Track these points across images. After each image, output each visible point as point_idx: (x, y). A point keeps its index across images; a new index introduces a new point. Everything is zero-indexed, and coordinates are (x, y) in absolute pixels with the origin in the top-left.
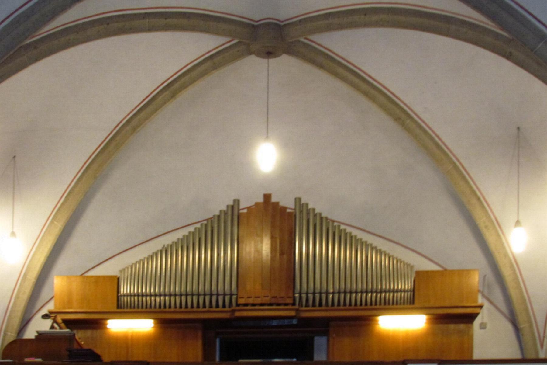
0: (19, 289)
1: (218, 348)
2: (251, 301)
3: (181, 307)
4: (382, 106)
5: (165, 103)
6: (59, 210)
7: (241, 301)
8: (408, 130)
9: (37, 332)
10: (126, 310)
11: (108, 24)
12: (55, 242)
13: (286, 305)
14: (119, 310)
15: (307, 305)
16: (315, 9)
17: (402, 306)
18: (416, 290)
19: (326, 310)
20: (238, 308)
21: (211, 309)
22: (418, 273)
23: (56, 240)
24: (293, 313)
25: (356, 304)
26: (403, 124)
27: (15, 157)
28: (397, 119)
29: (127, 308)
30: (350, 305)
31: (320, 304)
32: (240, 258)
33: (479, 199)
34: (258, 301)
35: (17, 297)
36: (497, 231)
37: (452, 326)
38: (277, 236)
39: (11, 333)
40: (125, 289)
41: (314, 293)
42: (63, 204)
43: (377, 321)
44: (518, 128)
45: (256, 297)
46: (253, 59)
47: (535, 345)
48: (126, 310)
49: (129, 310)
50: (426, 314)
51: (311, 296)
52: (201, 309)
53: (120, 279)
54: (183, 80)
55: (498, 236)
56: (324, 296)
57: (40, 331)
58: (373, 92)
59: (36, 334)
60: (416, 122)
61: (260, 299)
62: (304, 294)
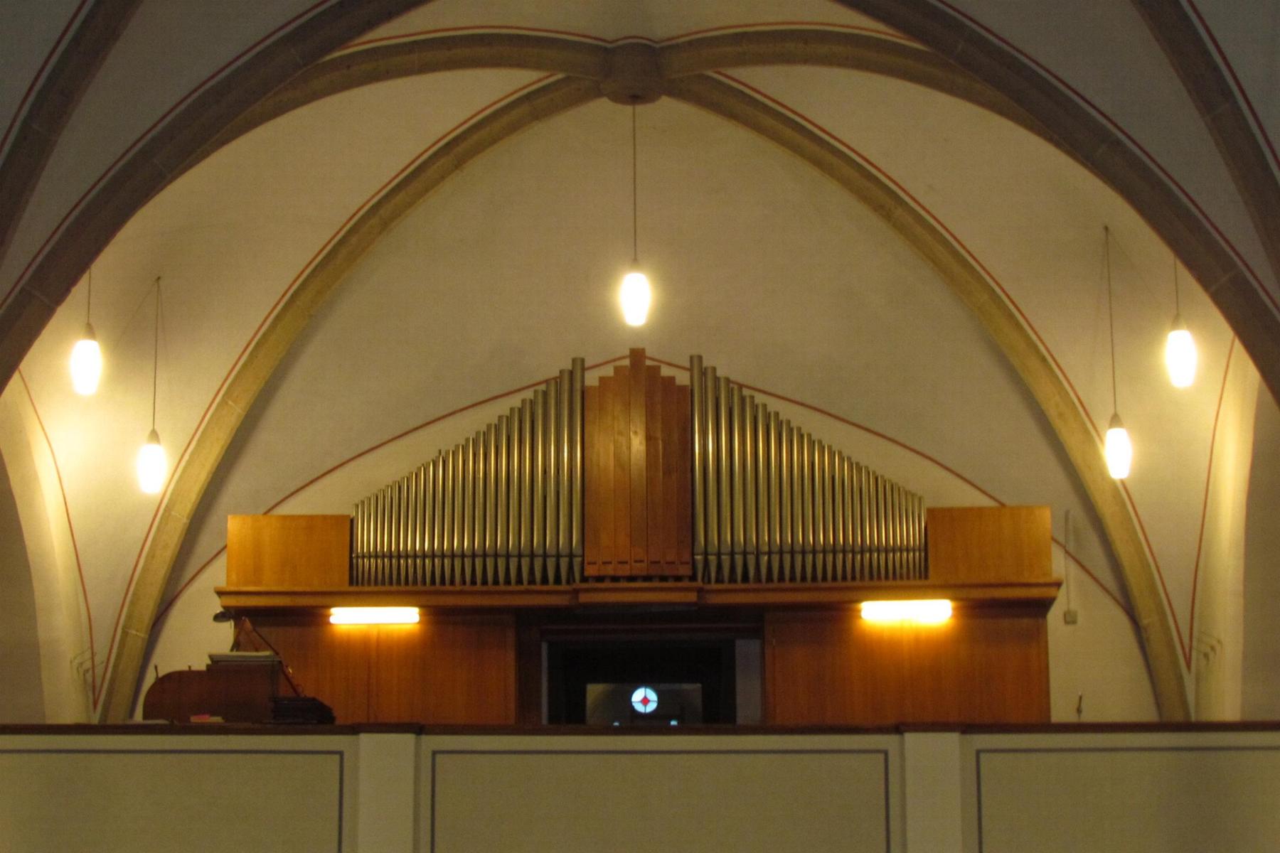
0: (154, 540)
1: (545, 664)
2: (609, 571)
3: (473, 582)
4: (845, 183)
5: (443, 178)
6: (237, 377)
7: (591, 571)
8: (900, 228)
9: (211, 657)
10: (366, 589)
11: (349, 67)
12: (229, 442)
13: (678, 578)
14: (353, 589)
17: (905, 582)
18: (930, 545)
19: (755, 591)
21: (533, 587)
22: (932, 513)
24: (692, 597)
26: (888, 216)
27: (159, 278)
28: (878, 208)
29: (369, 584)
30: (804, 578)
32: (586, 480)
33: (1044, 360)
34: (625, 571)
35: (152, 555)
36: (1083, 424)
37: (1006, 623)
38: (659, 435)
39: (137, 631)
41: (732, 554)
42: (245, 365)
43: (859, 611)
44: (1106, 229)
45: (620, 563)
48: (366, 589)
49: (372, 588)
50: (953, 599)
51: (726, 559)
52: (513, 587)
53: (355, 522)
55: (1087, 432)
57: (217, 656)
58: (830, 158)
61: (627, 567)
62: (712, 554)
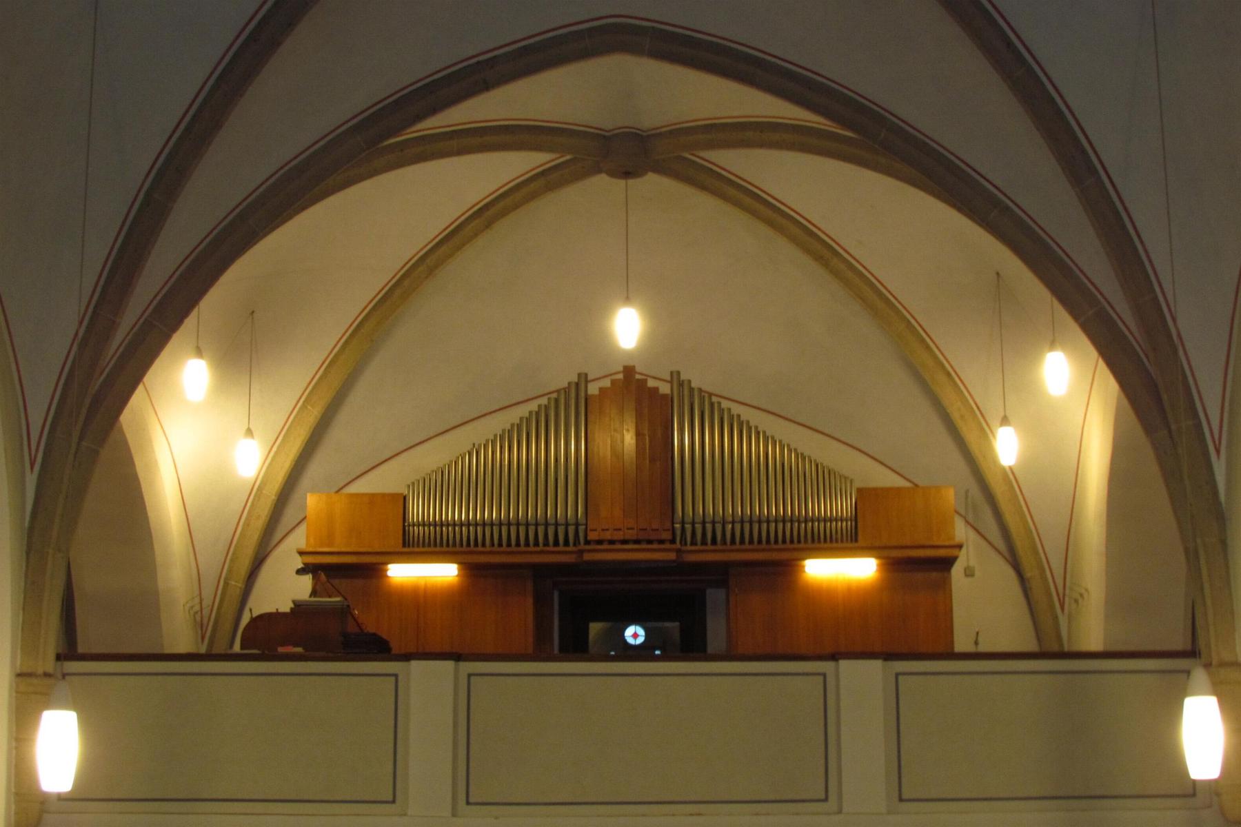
0: (249, 512)
1: (556, 607)
2: (608, 535)
4: (793, 239)
6: (314, 388)
7: (592, 536)
8: (836, 273)
9: (294, 602)
10: (416, 549)
11: (402, 150)
13: (661, 542)
14: (406, 550)
15: (693, 543)
16: (692, 118)
17: (840, 545)
19: (723, 551)
20: (587, 547)
21: (547, 549)
22: (860, 491)
23: (309, 435)
24: (672, 556)
25: (768, 541)
27: (253, 312)
28: (819, 259)
30: (760, 542)
31: (714, 542)
33: (949, 374)
34: (619, 536)
35: (247, 524)
38: (646, 432)
40: (417, 510)
41: (704, 523)
42: (321, 378)
43: (803, 567)
46: (601, 182)
47: (1052, 606)
48: (416, 549)
50: (877, 557)
51: (699, 527)
53: (407, 498)
54: (501, 204)
55: (982, 429)
56: (719, 528)
59: (292, 606)
60: (845, 261)
